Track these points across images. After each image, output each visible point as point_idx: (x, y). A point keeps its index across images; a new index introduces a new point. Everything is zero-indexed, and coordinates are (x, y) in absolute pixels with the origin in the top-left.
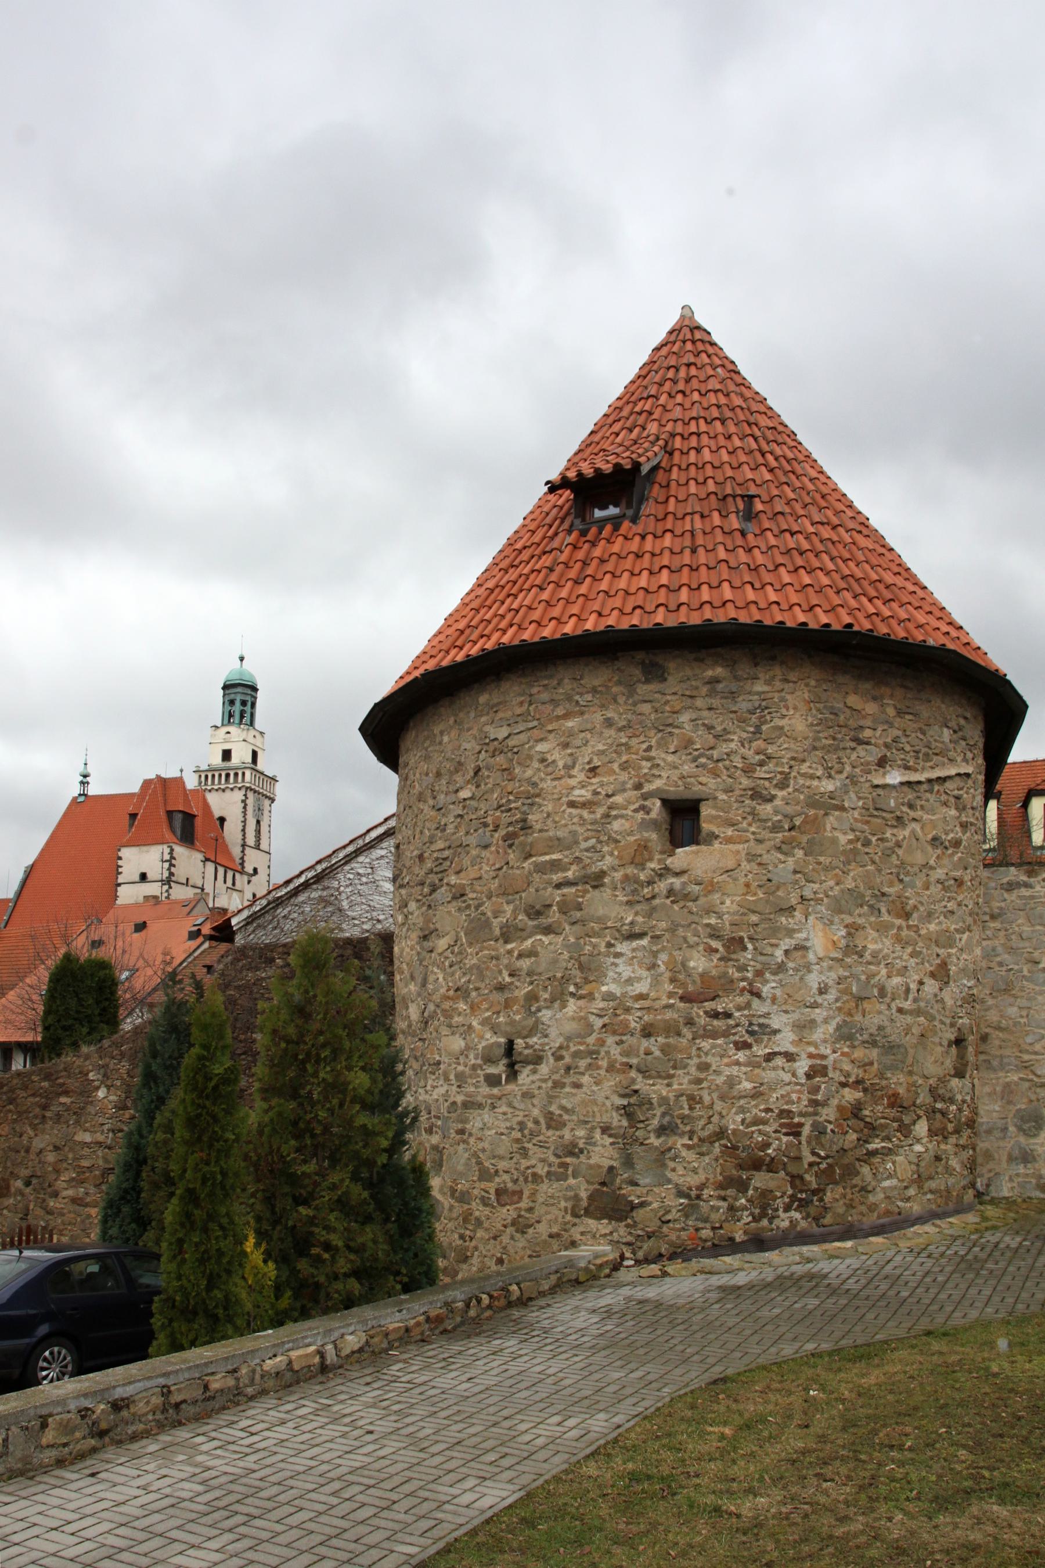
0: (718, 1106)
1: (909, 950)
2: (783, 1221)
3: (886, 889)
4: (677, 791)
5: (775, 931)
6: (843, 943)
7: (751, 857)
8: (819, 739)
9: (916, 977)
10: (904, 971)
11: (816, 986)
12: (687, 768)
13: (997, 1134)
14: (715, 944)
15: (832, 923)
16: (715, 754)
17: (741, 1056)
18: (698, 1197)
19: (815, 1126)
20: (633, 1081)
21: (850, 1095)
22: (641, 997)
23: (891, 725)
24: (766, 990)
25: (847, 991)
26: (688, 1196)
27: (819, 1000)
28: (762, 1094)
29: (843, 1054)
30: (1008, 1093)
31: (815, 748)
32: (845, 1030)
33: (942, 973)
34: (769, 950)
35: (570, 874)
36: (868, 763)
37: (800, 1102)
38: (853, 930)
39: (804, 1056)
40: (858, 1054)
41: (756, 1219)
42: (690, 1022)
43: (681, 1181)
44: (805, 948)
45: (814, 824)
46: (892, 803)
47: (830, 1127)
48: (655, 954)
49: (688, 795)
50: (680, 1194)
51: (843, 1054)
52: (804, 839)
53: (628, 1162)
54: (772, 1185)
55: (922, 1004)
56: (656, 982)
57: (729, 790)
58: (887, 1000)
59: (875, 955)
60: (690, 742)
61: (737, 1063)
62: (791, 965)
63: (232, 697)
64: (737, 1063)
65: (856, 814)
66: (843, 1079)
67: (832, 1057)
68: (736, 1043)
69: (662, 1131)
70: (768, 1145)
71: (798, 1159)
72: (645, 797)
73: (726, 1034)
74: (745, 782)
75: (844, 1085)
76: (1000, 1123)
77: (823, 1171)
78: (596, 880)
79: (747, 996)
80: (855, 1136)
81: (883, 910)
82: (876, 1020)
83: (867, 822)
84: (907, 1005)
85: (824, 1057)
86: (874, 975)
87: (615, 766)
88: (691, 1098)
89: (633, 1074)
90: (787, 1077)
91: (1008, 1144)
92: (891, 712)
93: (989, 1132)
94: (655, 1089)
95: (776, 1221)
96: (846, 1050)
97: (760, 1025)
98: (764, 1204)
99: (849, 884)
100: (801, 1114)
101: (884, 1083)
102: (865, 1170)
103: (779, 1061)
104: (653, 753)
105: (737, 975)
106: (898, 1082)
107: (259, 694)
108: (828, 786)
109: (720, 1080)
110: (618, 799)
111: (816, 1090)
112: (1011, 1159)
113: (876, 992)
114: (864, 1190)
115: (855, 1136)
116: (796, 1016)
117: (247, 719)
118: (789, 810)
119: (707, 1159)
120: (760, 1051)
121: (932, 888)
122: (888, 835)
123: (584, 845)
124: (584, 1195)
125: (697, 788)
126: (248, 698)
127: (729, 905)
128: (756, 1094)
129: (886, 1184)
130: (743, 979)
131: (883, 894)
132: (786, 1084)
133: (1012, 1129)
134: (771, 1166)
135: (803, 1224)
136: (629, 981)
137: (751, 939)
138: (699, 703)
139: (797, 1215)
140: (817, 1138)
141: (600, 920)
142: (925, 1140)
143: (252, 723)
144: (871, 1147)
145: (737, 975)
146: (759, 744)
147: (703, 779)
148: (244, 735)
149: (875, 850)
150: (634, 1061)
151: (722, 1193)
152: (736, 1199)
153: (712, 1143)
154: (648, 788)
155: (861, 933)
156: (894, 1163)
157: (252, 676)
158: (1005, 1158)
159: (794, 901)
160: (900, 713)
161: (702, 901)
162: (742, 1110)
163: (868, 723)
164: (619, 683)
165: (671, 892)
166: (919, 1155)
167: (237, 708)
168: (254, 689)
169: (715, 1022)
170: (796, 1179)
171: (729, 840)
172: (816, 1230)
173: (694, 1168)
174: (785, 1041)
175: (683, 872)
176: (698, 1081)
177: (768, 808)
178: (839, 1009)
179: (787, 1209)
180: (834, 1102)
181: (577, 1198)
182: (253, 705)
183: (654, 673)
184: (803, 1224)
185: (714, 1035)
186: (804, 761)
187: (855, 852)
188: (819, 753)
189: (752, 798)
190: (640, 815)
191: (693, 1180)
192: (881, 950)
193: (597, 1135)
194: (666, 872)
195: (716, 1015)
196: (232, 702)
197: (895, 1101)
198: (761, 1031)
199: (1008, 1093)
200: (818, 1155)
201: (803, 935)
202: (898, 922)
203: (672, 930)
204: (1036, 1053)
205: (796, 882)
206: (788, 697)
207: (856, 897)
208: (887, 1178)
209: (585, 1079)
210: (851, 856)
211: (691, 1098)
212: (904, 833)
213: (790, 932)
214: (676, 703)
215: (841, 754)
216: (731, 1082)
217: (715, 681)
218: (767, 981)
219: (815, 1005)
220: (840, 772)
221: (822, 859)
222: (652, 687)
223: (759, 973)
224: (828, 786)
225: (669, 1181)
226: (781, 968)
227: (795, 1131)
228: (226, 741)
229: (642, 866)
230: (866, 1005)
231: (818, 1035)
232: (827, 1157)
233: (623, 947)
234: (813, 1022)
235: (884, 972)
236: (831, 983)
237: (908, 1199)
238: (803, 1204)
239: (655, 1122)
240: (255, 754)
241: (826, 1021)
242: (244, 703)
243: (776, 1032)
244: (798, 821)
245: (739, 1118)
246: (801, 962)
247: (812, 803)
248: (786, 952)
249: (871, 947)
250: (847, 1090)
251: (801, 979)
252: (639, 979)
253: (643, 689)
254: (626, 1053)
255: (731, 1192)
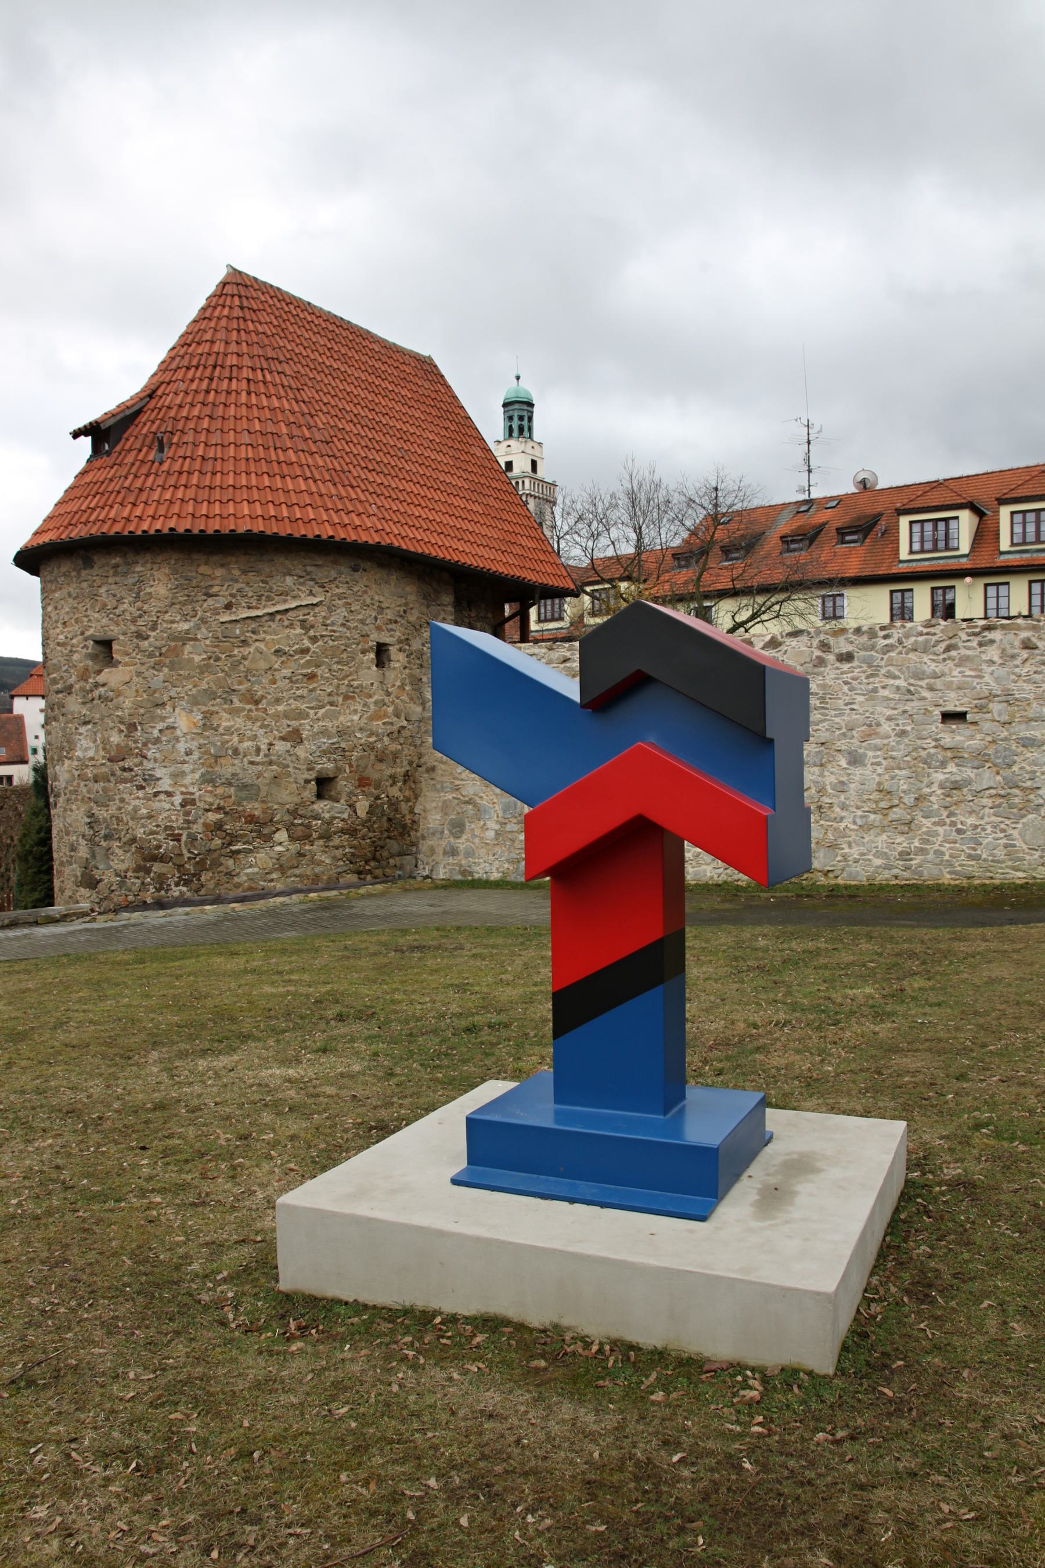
0: (131, 823)
1: (259, 724)
2: (175, 891)
3: (236, 687)
4: (100, 635)
5: (153, 718)
6: (201, 723)
7: (139, 674)
8: (177, 598)
9: (266, 741)
10: (255, 738)
11: (183, 750)
12: (105, 621)
13: (438, 836)
14: (123, 727)
15: (192, 711)
16: (117, 611)
17: (140, 794)
18: (126, 877)
19: (189, 835)
20: (92, 808)
21: (212, 817)
22: (92, 759)
23: (237, 581)
24: (150, 754)
25: (207, 752)
26: (120, 876)
27: (187, 759)
28: (153, 816)
29: (206, 791)
30: (445, 808)
31: (173, 604)
32: (208, 777)
33: (295, 737)
34: (150, 730)
35: (59, 686)
36: (216, 609)
37: (178, 821)
38: (208, 715)
39: (178, 793)
40: (220, 791)
41: (158, 890)
42: (113, 774)
43: (116, 867)
44: (174, 728)
45: (176, 652)
46: (238, 632)
47: (199, 836)
48: (95, 733)
49: (106, 638)
50: (117, 875)
51: (206, 791)
52: (167, 661)
53: (94, 856)
54: (164, 870)
55: (274, 758)
56: (97, 751)
57: (124, 634)
58: (241, 756)
59: (227, 729)
60: (105, 605)
61: (138, 798)
62: (164, 738)
63: (511, 413)
64: (138, 798)
65: (208, 642)
66: (207, 807)
67: (197, 794)
68: (137, 786)
69: (106, 837)
70: (160, 847)
71: (181, 855)
72: (86, 639)
73: (131, 781)
74: (133, 628)
75: (207, 810)
76: (440, 828)
77: (198, 863)
78: (68, 690)
79: (140, 759)
80: (219, 842)
81: (235, 700)
82: (231, 770)
83: (216, 646)
84: (258, 759)
85: (193, 794)
86: (227, 742)
87: (73, 621)
88: (117, 818)
89: (92, 804)
90: (167, 806)
91: (444, 843)
92: (236, 573)
93: (433, 834)
94: (102, 813)
95: (170, 893)
96: (210, 788)
97: (150, 775)
98: (161, 882)
99: (204, 686)
100: (179, 829)
101: (241, 808)
102: (231, 862)
103: (162, 797)
104: (89, 613)
105: (133, 745)
106: (255, 808)
107: (535, 409)
108: (186, 626)
109: (130, 808)
110: (74, 641)
111: (188, 813)
112: (445, 853)
113: (230, 752)
114: (230, 874)
115: (219, 842)
116: (172, 769)
117: (526, 433)
118: (158, 644)
119: (128, 854)
120: (149, 790)
121: (279, 683)
122: (236, 652)
123: (64, 668)
124: (79, 874)
125: (110, 633)
126: (525, 413)
127: (128, 704)
128: (150, 817)
129: (249, 871)
130: (137, 748)
131: (234, 691)
132: (168, 810)
133: (446, 832)
134: (162, 859)
135: (189, 894)
136: (86, 749)
137: (140, 723)
138: (111, 580)
139: (185, 889)
140: (191, 842)
141: (72, 713)
142: (285, 844)
143: (530, 437)
144: (233, 848)
145: (133, 745)
146: (139, 604)
147: (112, 628)
148: (522, 447)
149: (225, 663)
150: (92, 796)
151: (137, 875)
152: (144, 878)
153: (130, 845)
154: (88, 633)
155: (215, 716)
156: (255, 858)
157: (527, 392)
158: (441, 852)
159: (165, 699)
160: (244, 572)
161: (115, 701)
162: (143, 826)
163: (218, 582)
164: (74, 570)
165: (100, 697)
166: (280, 853)
167: (515, 424)
168: (531, 405)
169: (125, 774)
170: (179, 867)
171: (126, 665)
172: (197, 898)
173: (123, 860)
174: (165, 784)
175: (104, 685)
176: (120, 809)
177: (146, 643)
178: (202, 764)
179: (177, 884)
180: (201, 821)
181: (76, 876)
182: (530, 419)
183: (89, 564)
184: (189, 894)
185: (125, 781)
186: (166, 612)
187: (208, 666)
188: (177, 606)
189: (137, 637)
190: (84, 651)
191: (122, 867)
192: (232, 726)
193: (80, 840)
194: (97, 685)
195: (124, 769)
196: (511, 418)
197: (251, 819)
198: (151, 779)
199: (445, 808)
200: (193, 853)
201: (172, 720)
202: (248, 707)
203: (102, 719)
204: (462, 780)
205: (166, 688)
206: (155, 573)
207: (211, 695)
208: (250, 867)
209: (74, 807)
210: (204, 669)
211: (117, 818)
212: (246, 651)
213: (163, 719)
214: (98, 582)
215: (194, 605)
216: (136, 809)
217: (116, 566)
218: (150, 749)
219: (184, 762)
220: (195, 616)
221: (181, 672)
222: (87, 572)
223: (145, 744)
224: (186, 626)
225: (111, 867)
226: (157, 741)
227: (177, 838)
228: (507, 454)
229: (86, 681)
230: (222, 761)
231: (188, 780)
232: (199, 854)
233: (83, 730)
234: (184, 772)
235: (236, 739)
236: (193, 748)
237: (272, 880)
238: (187, 883)
239: (103, 832)
240: (534, 464)
241: (193, 771)
242: (521, 418)
243: (159, 779)
244: (164, 650)
245: (142, 830)
246: (171, 736)
247: (173, 638)
248: (160, 731)
249: (224, 724)
250: (210, 813)
251: (173, 746)
252: (90, 748)
253: (84, 573)
254: (89, 792)
255: (141, 874)
